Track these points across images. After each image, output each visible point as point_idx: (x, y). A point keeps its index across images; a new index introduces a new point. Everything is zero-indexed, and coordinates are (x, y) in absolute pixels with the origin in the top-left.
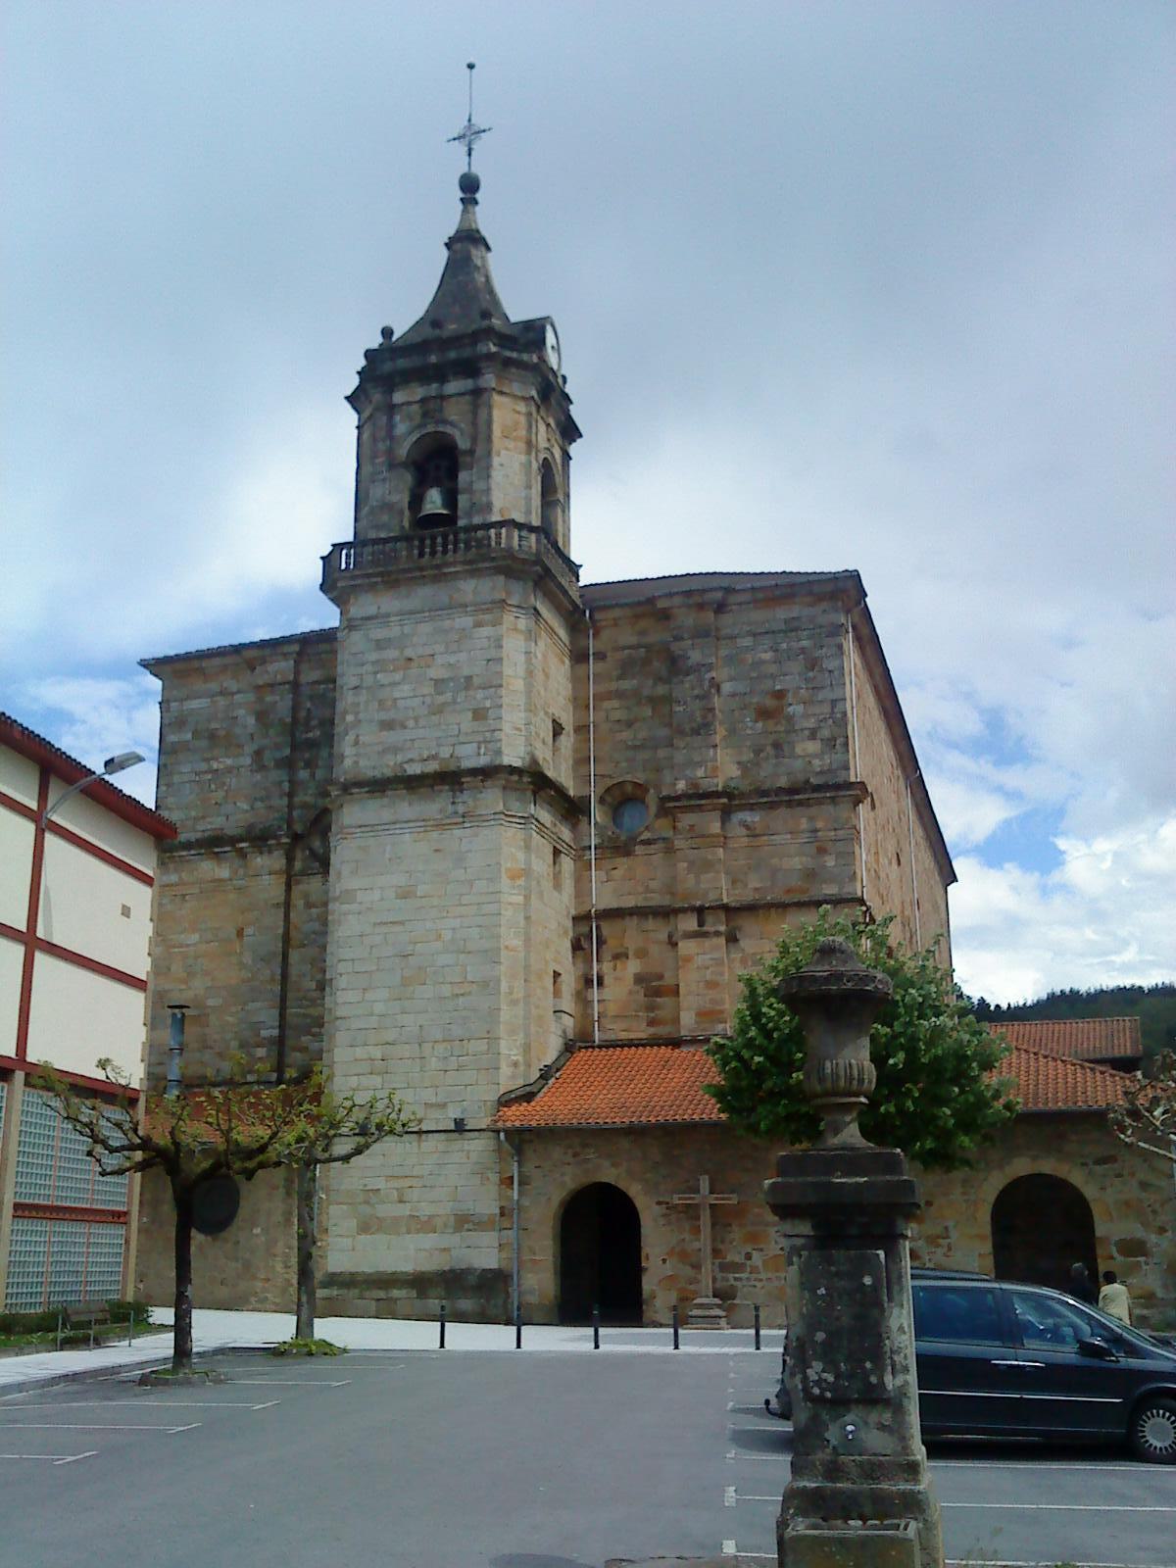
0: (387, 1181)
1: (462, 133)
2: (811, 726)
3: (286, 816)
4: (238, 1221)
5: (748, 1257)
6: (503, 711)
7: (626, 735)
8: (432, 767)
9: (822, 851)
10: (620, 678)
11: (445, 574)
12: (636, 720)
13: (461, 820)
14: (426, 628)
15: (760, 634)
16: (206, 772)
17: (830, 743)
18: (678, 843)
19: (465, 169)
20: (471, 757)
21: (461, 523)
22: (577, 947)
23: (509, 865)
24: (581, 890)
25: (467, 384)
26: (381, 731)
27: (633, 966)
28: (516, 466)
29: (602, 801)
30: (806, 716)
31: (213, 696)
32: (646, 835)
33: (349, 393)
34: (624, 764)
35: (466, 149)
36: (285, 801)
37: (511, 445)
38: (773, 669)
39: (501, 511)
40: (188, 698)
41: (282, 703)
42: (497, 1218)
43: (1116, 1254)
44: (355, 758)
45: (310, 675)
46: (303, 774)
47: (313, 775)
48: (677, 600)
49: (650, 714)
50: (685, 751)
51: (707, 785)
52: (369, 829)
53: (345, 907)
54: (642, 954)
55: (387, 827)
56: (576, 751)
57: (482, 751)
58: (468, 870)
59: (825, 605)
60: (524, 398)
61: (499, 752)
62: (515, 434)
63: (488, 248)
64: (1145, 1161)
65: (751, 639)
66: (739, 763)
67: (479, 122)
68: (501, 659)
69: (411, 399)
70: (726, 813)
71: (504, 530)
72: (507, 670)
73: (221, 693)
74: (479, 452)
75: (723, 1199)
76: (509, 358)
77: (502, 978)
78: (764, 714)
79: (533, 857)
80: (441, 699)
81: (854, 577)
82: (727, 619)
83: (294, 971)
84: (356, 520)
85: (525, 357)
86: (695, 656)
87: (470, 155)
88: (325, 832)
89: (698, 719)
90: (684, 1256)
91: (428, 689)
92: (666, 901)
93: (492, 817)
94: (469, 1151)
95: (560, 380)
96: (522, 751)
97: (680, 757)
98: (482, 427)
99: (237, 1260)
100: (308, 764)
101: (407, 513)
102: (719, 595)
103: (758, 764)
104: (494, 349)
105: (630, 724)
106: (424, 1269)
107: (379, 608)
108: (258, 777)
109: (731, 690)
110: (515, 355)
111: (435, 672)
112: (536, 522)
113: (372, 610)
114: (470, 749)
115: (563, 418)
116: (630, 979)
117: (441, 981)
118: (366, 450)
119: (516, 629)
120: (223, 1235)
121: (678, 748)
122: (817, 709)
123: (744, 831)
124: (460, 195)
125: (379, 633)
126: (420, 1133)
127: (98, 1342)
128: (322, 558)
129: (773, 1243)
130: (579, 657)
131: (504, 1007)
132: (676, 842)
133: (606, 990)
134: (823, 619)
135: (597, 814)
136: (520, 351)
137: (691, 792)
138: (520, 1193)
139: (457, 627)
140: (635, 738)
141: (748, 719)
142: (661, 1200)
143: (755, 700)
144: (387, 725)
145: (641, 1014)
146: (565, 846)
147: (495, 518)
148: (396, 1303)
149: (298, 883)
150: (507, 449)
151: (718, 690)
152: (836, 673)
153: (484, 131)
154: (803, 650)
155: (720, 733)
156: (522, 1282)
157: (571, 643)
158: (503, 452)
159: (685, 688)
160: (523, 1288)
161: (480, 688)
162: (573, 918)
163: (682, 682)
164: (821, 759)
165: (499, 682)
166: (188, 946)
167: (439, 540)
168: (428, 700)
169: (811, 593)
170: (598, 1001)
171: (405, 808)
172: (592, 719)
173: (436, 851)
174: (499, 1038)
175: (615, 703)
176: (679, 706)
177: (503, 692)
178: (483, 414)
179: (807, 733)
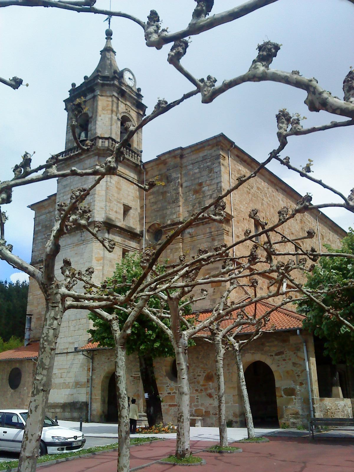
0: (58, 370)
4: (21, 385)
6: (96, 202)
7: (155, 207)
9: (213, 240)
11: (81, 159)
13: (82, 242)
15: (195, 163)
16: (44, 238)
28: (107, 119)
30: (209, 190)
31: (46, 214)
34: (154, 217)
37: (105, 112)
38: (198, 175)
40: (41, 215)
42: (86, 383)
43: (283, 395)
48: (167, 156)
49: (162, 198)
50: (170, 210)
58: (84, 259)
59: (215, 148)
62: (107, 108)
63: (114, 52)
64: (295, 353)
65: (192, 165)
66: (188, 211)
73: (48, 213)
74: (94, 117)
78: (196, 192)
82: (184, 160)
89: (174, 197)
93: (91, 240)
94: (80, 359)
97: (168, 212)
98: (95, 108)
99: (20, 398)
102: (179, 151)
106: (66, 402)
109: (186, 185)
115: (135, 102)
121: (168, 209)
122: (211, 187)
126: (67, 353)
129: (165, 391)
134: (214, 154)
135: (146, 237)
136: (110, 81)
141: (191, 195)
143: (193, 188)
146: (132, 248)
148: (57, 414)
150: (104, 114)
152: (218, 173)
154: (208, 167)
155: (181, 202)
158: (102, 115)
160: (92, 409)
163: (170, 185)
166: (38, 295)
169: (209, 145)
172: (144, 203)
173: (76, 254)
175: (152, 197)
179: (209, 197)
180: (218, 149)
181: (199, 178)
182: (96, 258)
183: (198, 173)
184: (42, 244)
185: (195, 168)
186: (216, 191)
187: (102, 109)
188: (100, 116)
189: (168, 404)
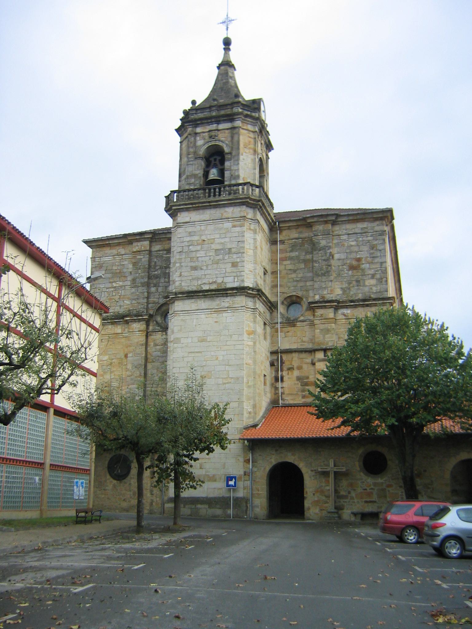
1: (224, 21)
2: (372, 273)
3: (146, 307)
5: (349, 493)
7: (294, 276)
8: (213, 287)
10: (291, 251)
12: (298, 269)
14: (211, 227)
16: (110, 288)
17: (380, 280)
18: (316, 322)
19: (226, 36)
20: (231, 283)
21: (226, 183)
22: (272, 364)
23: (247, 329)
24: (274, 341)
25: (228, 125)
26: (191, 271)
27: (296, 373)
29: (283, 303)
30: (370, 269)
32: (302, 318)
33: (177, 128)
34: (293, 288)
35: (226, 27)
36: (145, 300)
38: (356, 249)
39: (243, 178)
41: (144, 259)
42: (243, 476)
44: (180, 282)
45: (156, 247)
46: (153, 289)
47: (157, 290)
50: (319, 283)
51: (329, 297)
52: (187, 312)
53: (176, 345)
54: (300, 368)
55: (194, 311)
56: (272, 282)
57: (236, 280)
58: (230, 331)
59: (378, 223)
60: (253, 132)
61: (243, 281)
63: (235, 70)
65: (347, 236)
66: (341, 288)
67: (231, 17)
68: (244, 241)
69: (204, 131)
70: (336, 308)
71: (245, 187)
72: (247, 246)
75: (339, 469)
76: (247, 114)
77: (244, 376)
79: (257, 325)
80: (218, 258)
81: (390, 211)
82: (337, 228)
83: (149, 373)
84: (180, 181)
85: (253, 114)
86: (323, 243)
87: (227, 30)
88: (165, 315)
90: (322, 492)
91: (212, 253)
92: (310, 346)
95: (266, 125)
96: (252, 280)
100: (155, 286)
101: (202, 178)
102: (333, 218)
103: (349, 289)
104: (240, 110)
105: (295, 271)
107: (190, 218)
108: (133, 290)
110: (249, 113)
111: (214, 246)
112: (257, 183)
113: (187, 219)
114: (230, 279)
116: (295, 379)
117: (218, 377)
118: (184, 152)
119: (250, 229)
120: (125, 480)
121: (316, 281)
122: (373, 266)
123: (344, 317)
124: (224, 47)
125: (190, 229)
127: (386, 268)
128: (166, 197)
130: (273, 242)
131: (245, 389)
132: (315, 321)
133: (284, 383)
134: (377, 228)
135: (281, 308)
137: (321, 300)
138: (253, 466)
139: (225, 227)
140: (297, 277)
142: (313, 469)
143: (348, 262)
144: (195, 268)
145: (299, 393)
147: (241, 181)
149: (151, 335)
150: (245, 152)
151: (333, 257)
153: (233, 20)
154: (369, 241)
156: (253, 502)
157: (270, 236)
158: (244, 154)
159: (318, 256)
160: (253, 505)
161: (235, 253)
162: (271, 353)
164: (377, 287)
165: (243, 251)
166: (104, 360)
167: (217, 190)
168: (212, 258)
170: (281, 387)
171: (203, 304)
173: (216, 322)
174: (243, 402)
175: (288, 262)
176: (316, 263)
177: (245, 255)
178: (236, 138)
179: (370, 276)
180: (383, 225)
181: (357, 252)
182: (246, 331)
183: (355, 246)
184: (107, 295)
185: (350, 240)
186: (380, 272)
187: (244, 146)
188: (242, 155)
189: (363, 500)
